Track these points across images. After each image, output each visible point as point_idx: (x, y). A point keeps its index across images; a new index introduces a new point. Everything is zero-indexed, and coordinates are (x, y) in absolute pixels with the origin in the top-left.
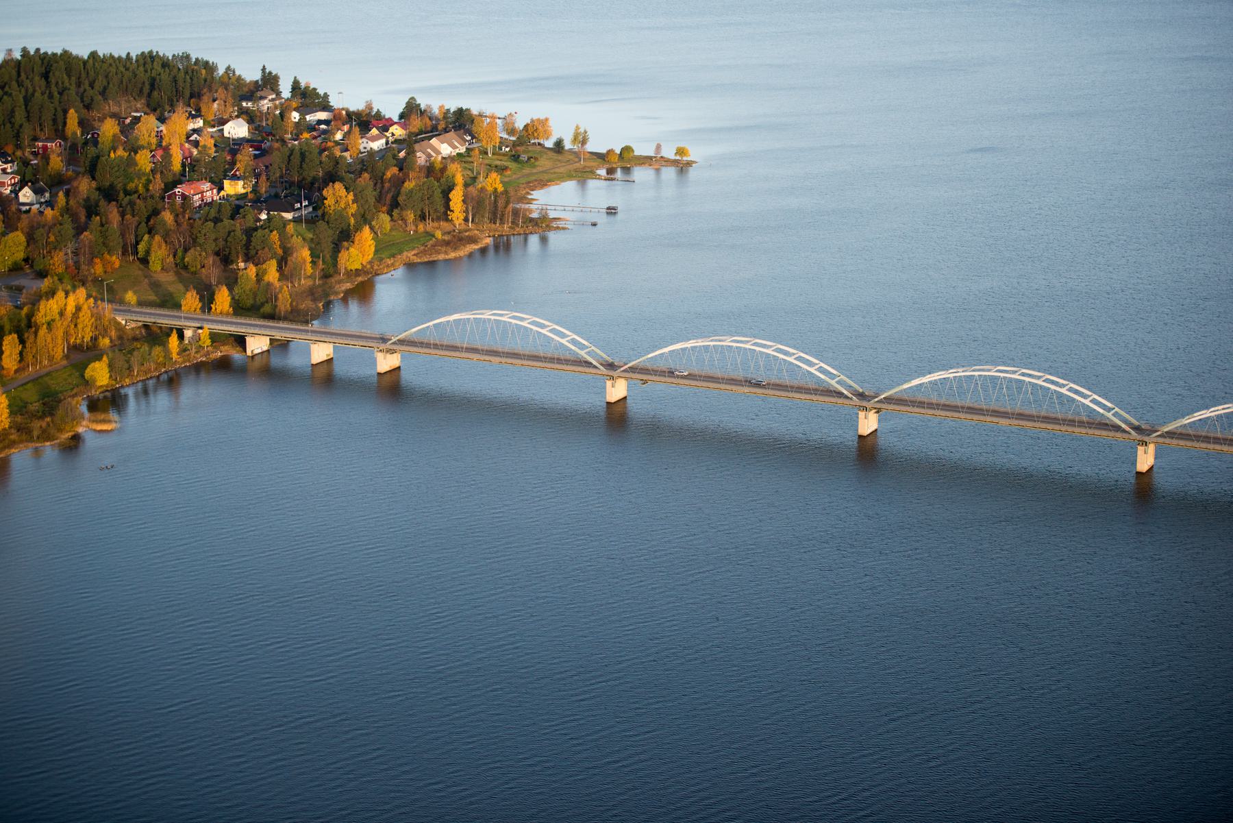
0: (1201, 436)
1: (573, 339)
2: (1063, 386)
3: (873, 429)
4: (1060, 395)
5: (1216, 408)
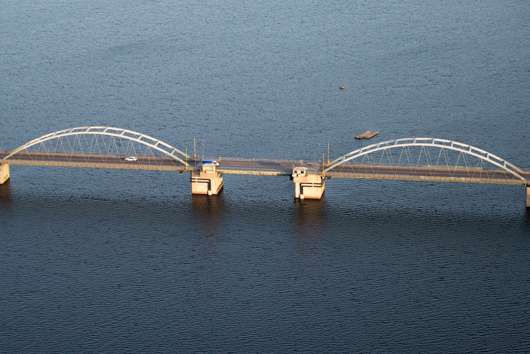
0: (396, 173)
1: (126, 133)
2: (120, 132)
3: (8, 178)
4: (136, 144)
5: (45, 136)
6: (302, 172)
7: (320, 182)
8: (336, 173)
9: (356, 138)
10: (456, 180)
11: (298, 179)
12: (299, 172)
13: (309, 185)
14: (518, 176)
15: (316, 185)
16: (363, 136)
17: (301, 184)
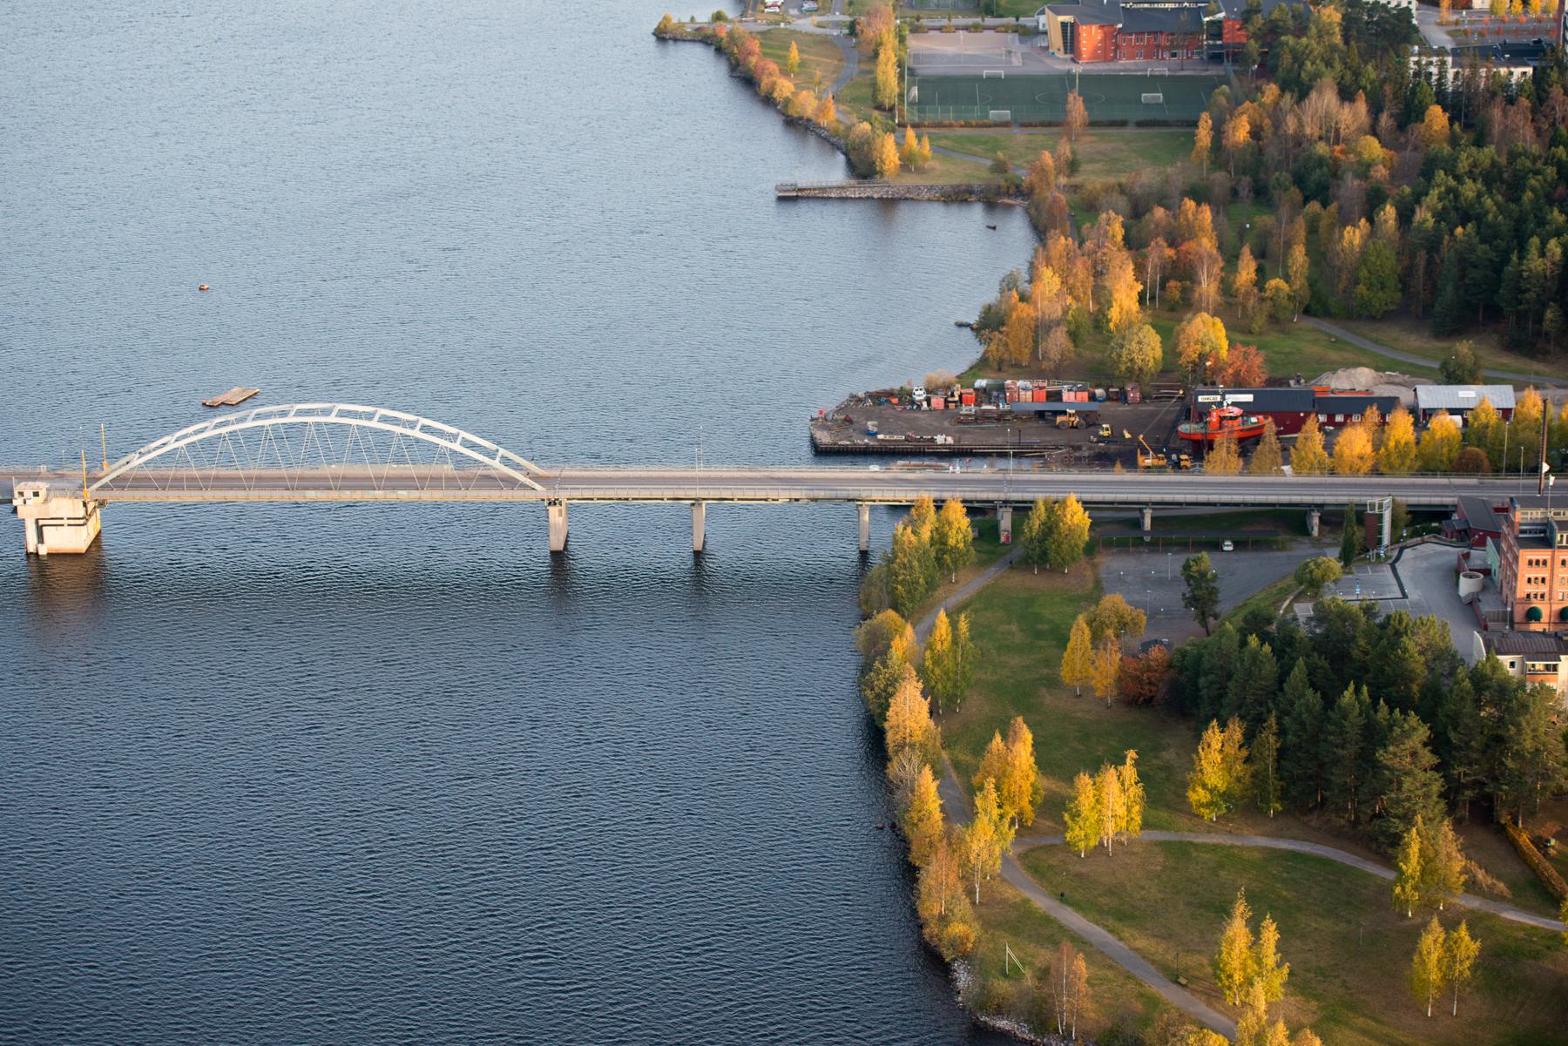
6: (36, 494)
7: (81, 513)
8: (116, 493)
9: (204, 404)
10: (388, 496)
11: (29, 510)
12: (28, 494)
13: (57, 522)
14: (528, 481)
15: (72, 522)
16: (221, 399)
17: (37, 520)
